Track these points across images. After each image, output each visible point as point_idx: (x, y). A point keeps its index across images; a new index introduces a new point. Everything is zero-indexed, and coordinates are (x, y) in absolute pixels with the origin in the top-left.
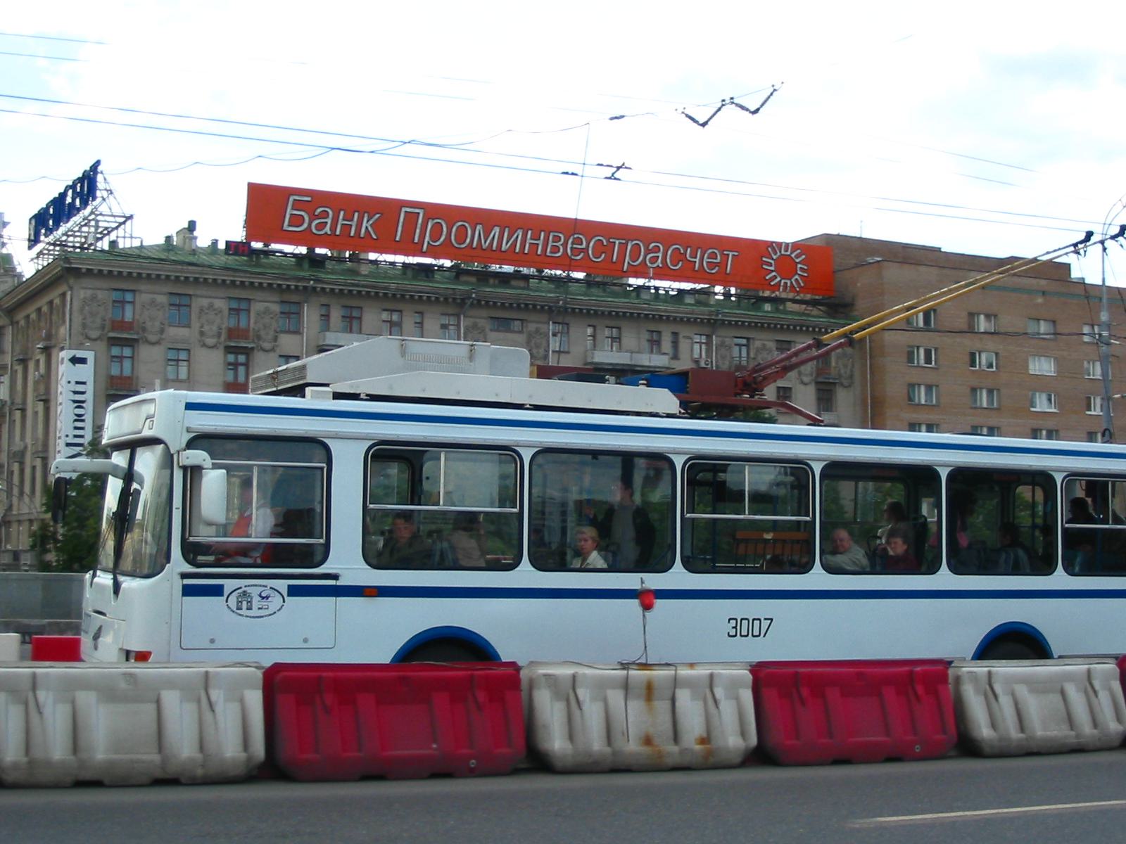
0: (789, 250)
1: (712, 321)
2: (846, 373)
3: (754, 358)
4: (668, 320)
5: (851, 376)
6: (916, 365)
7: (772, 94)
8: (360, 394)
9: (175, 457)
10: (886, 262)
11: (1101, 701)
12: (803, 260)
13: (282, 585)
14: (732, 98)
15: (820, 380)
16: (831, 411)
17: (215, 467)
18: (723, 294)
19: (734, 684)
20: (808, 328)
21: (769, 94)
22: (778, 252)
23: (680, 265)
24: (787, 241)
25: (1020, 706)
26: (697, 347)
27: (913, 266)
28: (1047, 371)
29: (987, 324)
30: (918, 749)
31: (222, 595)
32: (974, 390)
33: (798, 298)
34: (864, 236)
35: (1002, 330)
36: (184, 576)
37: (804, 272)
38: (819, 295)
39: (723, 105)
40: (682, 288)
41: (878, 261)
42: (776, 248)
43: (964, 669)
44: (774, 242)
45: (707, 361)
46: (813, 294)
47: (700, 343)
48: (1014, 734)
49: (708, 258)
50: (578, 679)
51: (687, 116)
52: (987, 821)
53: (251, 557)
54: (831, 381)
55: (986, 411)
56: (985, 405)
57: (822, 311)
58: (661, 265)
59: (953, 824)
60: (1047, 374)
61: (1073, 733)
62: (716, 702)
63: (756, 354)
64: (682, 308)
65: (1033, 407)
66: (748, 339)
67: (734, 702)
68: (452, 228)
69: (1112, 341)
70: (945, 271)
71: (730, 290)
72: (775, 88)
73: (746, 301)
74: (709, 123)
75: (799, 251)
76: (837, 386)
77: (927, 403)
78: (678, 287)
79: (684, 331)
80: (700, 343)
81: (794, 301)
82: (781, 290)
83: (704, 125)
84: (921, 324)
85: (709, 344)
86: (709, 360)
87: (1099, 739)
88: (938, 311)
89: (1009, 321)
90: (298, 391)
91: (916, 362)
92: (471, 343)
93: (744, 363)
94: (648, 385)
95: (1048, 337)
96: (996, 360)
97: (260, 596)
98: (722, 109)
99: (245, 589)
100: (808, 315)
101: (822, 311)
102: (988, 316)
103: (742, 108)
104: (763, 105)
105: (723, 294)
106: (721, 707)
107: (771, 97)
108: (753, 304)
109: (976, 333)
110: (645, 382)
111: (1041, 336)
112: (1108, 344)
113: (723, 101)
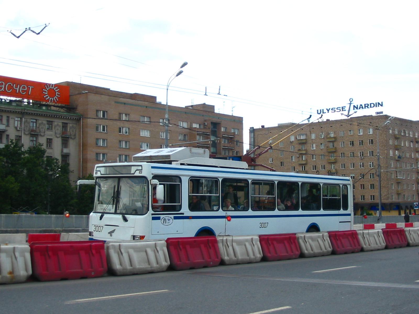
0: (53, 87)
1: (23, 113)
2: (73, 134)
3: (38, 127)
4: (5, 111)
5: (75, 135)
6: (99, 131)
7: (45, 27)
8: (184, 164)
9: (149, 182)
10: (89, 93)
11: (160, 255)
12: (58, 91)
13: (172, 216)
14: (30, 28)
15: (63, 136)
16: (67, 148)
17: (160, 184)
18: (27, 102)
19: (22, 252)
20: (57, 116)
21: (44, 27)
22: (49, 87)
23: (11, 91)
24: (53, 83)
25: (131, 257)
26: (16, 122)
27: (99, 95)
28: (147, 135)
29: (126, 118)
30: (93, 274)
31: (160, 219)
32: (120, 141)
33: (56, 105)
34: (82, 83)
35: (131, 120)
36: (152, 214)
37: (58, 95)
38: (64, 104)
39: (26, 30)
40: (11, 99)
41: (87, 93)
42: (48, 86)
43: (110, 244)
44: (48, 84)
45: (20, 128)
46: (61, 104)
47: (18, 121)
48: (129, 267)
49: (22, 88)
50: (228, 240)
51: (12, 33)
52: (117, 299)
53: (159, 209)
54: (67, 136)
55: (124, 149)
56: (124, 147)
57: (65, 110)
58: (3, 90)
59: (104, 301)
60: (147, 136)
61: (150, 266)
62: (16, 258)
63: (39, 126)
64: (11, 107)
65: (141, 148)
66: (36, 120)
67: (23, 258)
68: (6, 85)
69: (169, 125)
70: (111, 97)
71: (30, 101)
72: (46, 25)
73: (36, 105)
74: (20, 37)
75: (57, 87)
76: (39, 136)
77: (103, 146)
78: (10, 99)
79: (11, 116)
80: (18, 121)
81: (54, 106)
82: (50, 102)
83: (18, 37)
84: (102, 116)
85: (21, 121)
86: (21, 127)
87: (159, 268)
88: (108, 112)
89: (133, 117)
90: (170, 162)
91: (99, 130)
92: (204, 149)
93: (34, 129)
94: (232, 160)
95: (147, 123)
96: (129, 130)
97: (168, 219)
98: (26, 32)
99: (165, 218)
100: (60, 112)
101: (65, 110)
102: (126, 115)
103: (33, 32)
104: (41, 31)
105: (27, 102)
106: (123, 255)
107: (45, 28)
108: (39, 106)
109: (121, 120)
110: (232, 159)
111: (145, 122)
112: (168, 126)
113: (26, 29)
